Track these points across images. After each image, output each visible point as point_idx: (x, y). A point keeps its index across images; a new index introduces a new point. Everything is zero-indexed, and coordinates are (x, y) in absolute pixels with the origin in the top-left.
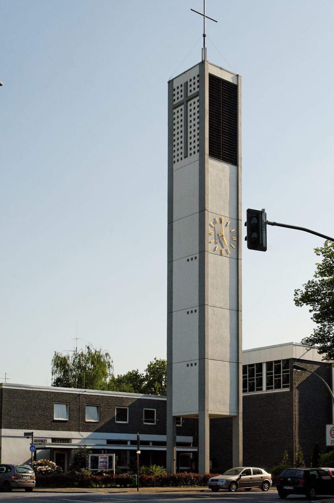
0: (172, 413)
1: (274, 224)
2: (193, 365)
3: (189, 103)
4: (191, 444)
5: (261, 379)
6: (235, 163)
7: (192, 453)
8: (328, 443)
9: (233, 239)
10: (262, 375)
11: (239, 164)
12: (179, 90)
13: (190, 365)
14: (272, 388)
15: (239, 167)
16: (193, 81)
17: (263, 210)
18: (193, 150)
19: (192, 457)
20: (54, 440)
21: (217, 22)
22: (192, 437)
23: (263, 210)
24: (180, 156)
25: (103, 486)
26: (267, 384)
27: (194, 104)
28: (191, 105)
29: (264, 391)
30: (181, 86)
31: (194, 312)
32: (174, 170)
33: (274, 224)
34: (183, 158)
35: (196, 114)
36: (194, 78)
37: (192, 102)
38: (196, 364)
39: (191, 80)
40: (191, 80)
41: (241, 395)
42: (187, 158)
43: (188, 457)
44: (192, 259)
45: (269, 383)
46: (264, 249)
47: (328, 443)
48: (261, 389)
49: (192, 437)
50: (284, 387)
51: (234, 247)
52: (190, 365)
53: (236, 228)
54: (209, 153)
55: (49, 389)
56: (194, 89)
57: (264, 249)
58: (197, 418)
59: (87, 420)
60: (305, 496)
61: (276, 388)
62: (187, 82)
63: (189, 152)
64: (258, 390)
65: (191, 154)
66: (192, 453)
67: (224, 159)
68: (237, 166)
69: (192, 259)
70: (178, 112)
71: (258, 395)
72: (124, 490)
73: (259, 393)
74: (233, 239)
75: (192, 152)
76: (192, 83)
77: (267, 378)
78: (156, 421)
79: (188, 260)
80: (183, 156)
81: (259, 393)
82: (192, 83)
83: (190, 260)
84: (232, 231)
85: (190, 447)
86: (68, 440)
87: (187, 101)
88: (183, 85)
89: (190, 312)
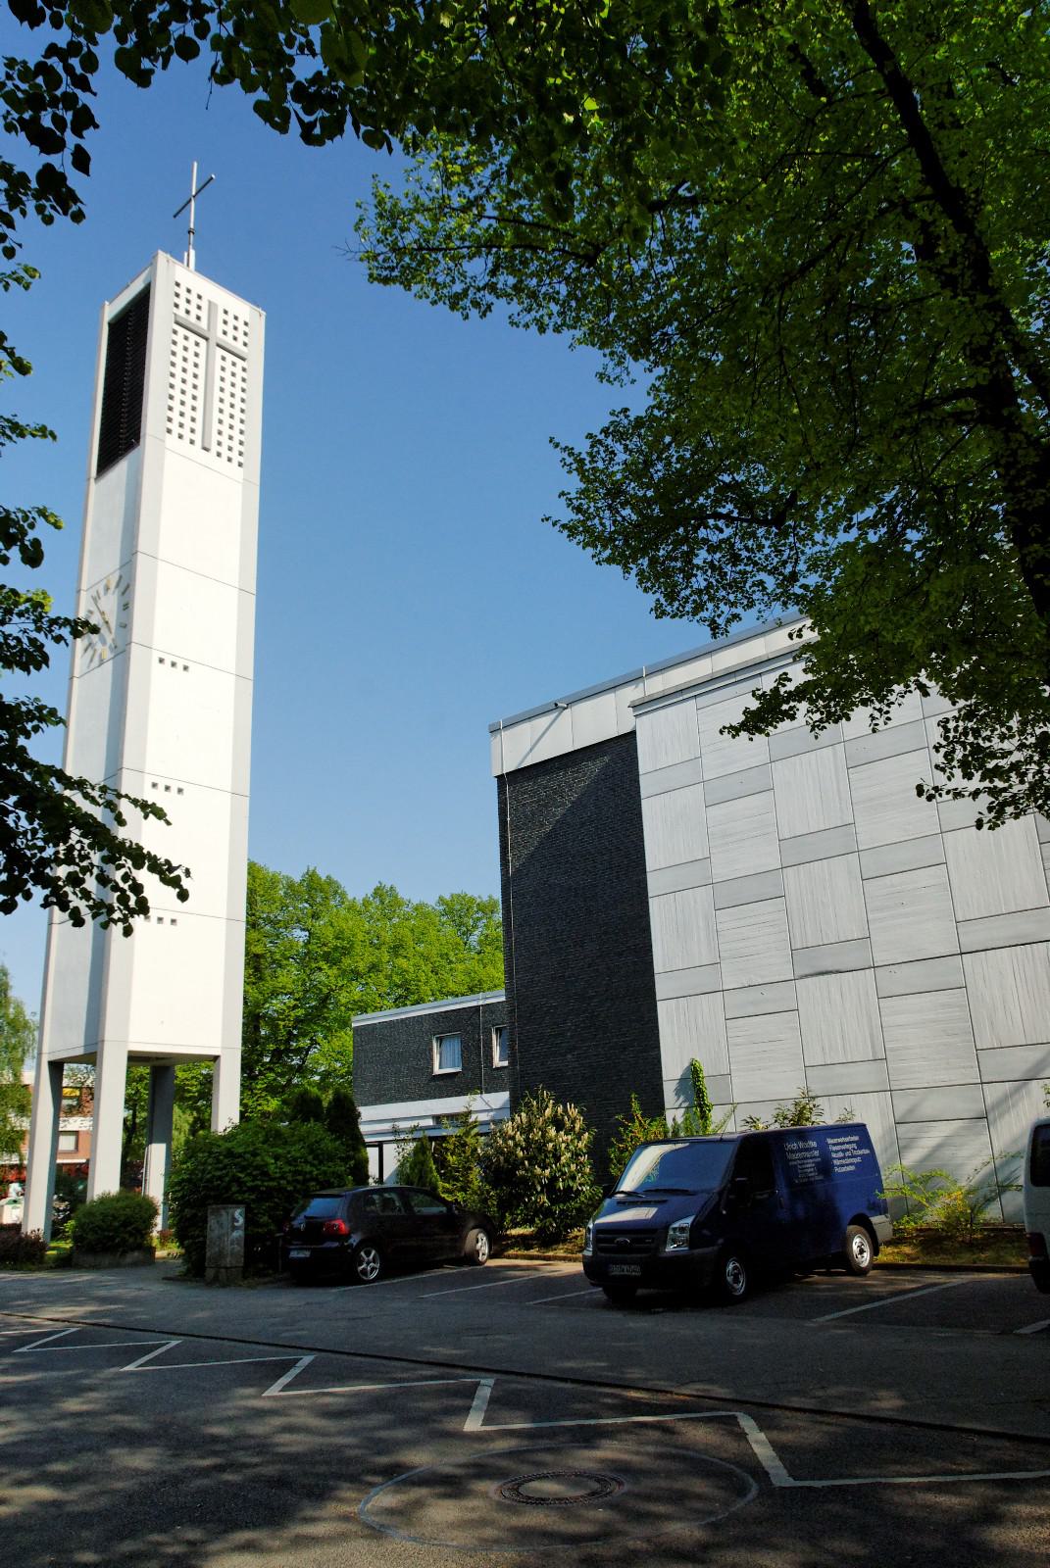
62: (243, 359)
63: (182, 331)
76: (238, 370)
82: (238, 370)
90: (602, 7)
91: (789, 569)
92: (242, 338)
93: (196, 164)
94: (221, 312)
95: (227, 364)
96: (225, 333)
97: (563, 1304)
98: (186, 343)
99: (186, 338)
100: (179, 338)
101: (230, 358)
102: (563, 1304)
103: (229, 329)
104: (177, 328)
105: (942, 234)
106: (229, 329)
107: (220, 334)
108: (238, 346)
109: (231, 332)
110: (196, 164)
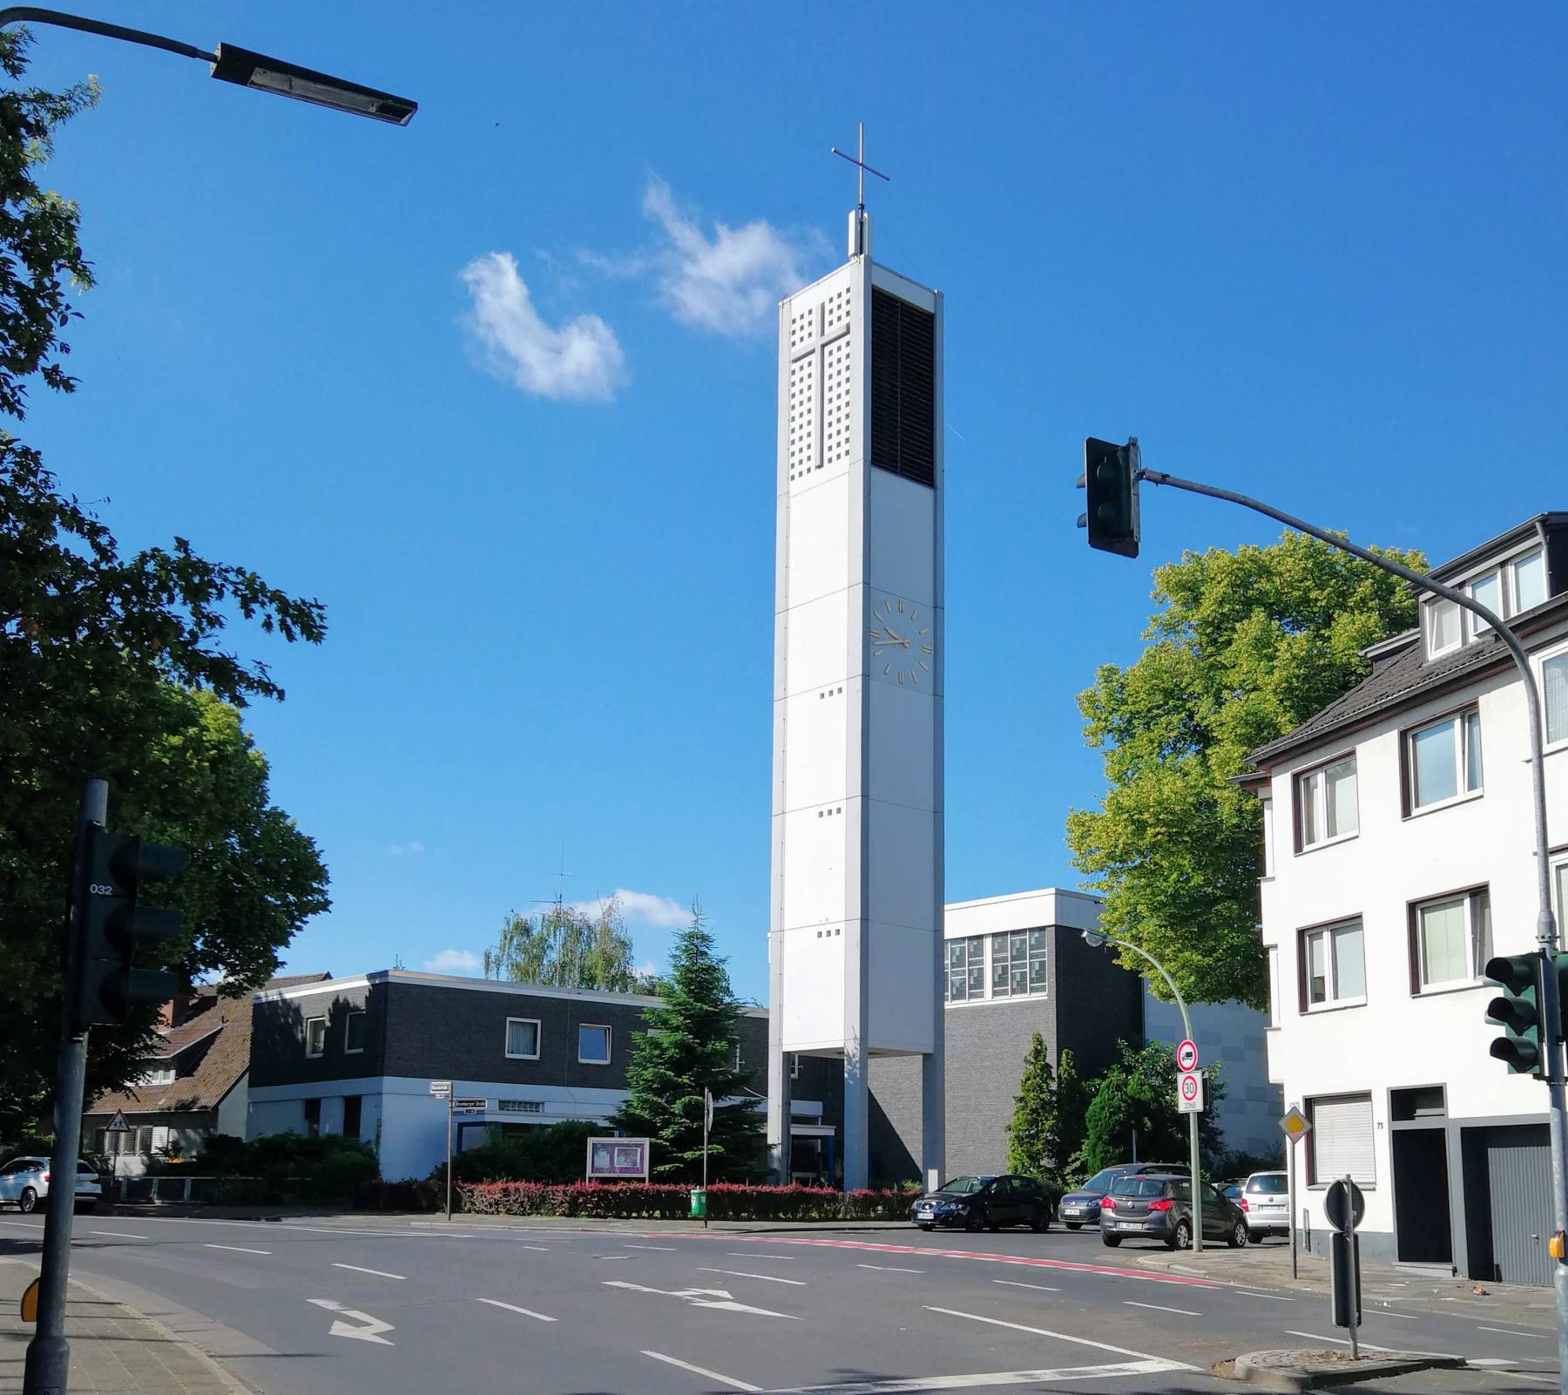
0: (781, 1045)
1: (1163, 479)
2: (833, 933)
3: (827, 349)
4: (818, 1118)
5: (981, 971)
6: (929, 482)
7: (819, 1141)
8: (1566, 1075)
10: (981, 962)
11: (938, 482)
12: (805, 322)
13: (824, 934)
14: (1005, 993)
16: (836, 302)
17: (1133, 443)
18: (835, 451)
19: (819, 1150)
20: (504, 1105)
24: (806, 465)
25: (634, 1215)
26: (995, 984)
27: (835, 353)
28: (831, 353)
29: (988, 998)
30: (810, 312)
31: (834, 812)
32: (791, 495)
33: (1163, 479)
35: (804, 450)
36: (840, 295)
38: (838, 932)
39: (831, 300)
40: (831, 300)
41: (1028, 970)
42: (821, 469)
43: (813, 1148)
44: (831, 693)
45: (1000, 981)
46: (1131, 550)
47: (1566, 1075)
48: (981, 995)
50: (1033, 989)
52: (824, 934)
53: (932, 625)
54: (872, 458)
56: (839, 318)
59: (581, 1061)
60: (964, 1229)
61: (1014, 992)
62: (823, 306)
63: (827, 455)
64: (972, 996)
65: (830, 460)
66: (819, 1141)
67: (903, 472)
69: (831, 693)
70: (802, 368)
71: (973, 1009)
72: (726, 1225)
75: (833, 454)
76: (834, 305)
77: (994, 969)
78: (740, 1064)
79: (822, 696)
82: (834, 305)
83: (827, 695)
84: (922, 632)
86: (535, 1106)
87: (823, 346)
89: (825, 813)
90: (2, 334)
91: (648, 1065)
92: (807, 318)
93: (361, 1050)
94: (794, 349)
95: (834, 317)
96: (810, 335)
97: (1309, 1278)
98: (834, 423)
99: (831, 312)
100: (833, 454)
101: (828, 318)
102: (1309, 1278)
103: (805, 333)
104: (826, 461)
105: (206, 634)
106: (805, 333)
107: (813, 338)
108: (815, 318)
109: (807, 330)
110: (361, 1050)
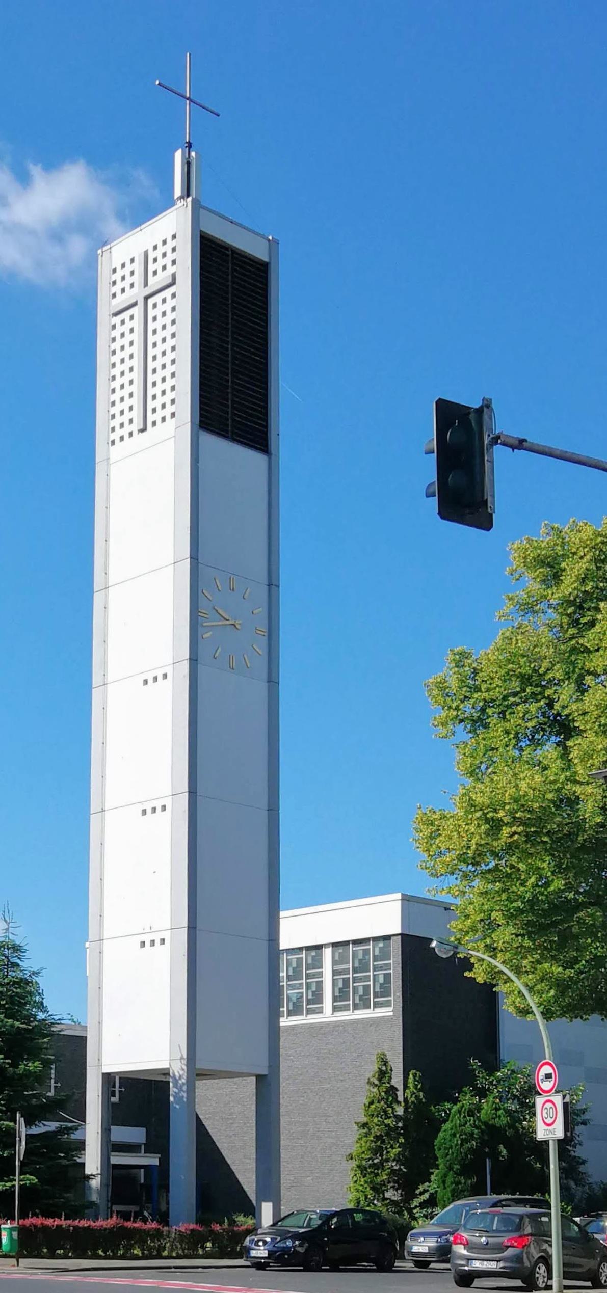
1: (520, 444)
3: (151, 302)
5: (320, 985)
7: (142, 1170)
9: (257, 632)
10: (320, 975)
11: (273, 448)
12: (127, 272)
13: (148, 944)
14: (346, 1008)
15: (273, 457)
17: (487, 405)
19: (142, 1181)
21: (218, 115)
22: (143, 1131)
23: (487, 405)
24: (128, 428)
26: (335, 999)
28: (155, 306)
29: (327, 1014)
32: (111, 461)
33: (520, 444)
34: (135, 433)
37: (158, 298)
39: (155, 248)
40: (155, 248)
41: (371, 983)
42: (144, 433)
43: (134, 1179)
45: (340, 996)
46: (485, 523)
49: (143, 1131)
50: (377, 1005)
51: (261, 653)
52: (148, 944)
53: (265, 605)
54: (201, 421)
55: (127, 238)
57: (485, 523)
58: (163, 1078)
61: (356, 1007)
62: (146, 254)
64: (310, 1011)
65: (154, 423)
66: (142, 1170)
68: (268, 456)
71: (311, 1026)
73: (314, 1019)
74: (257, 632)
75: (157, 417)
76: (158, 253)
80: (135, 427)
81: (314, 1019)
82: (158, 253)
85: (139, 1155)
87: (146, 298)
88: (136, 260)
